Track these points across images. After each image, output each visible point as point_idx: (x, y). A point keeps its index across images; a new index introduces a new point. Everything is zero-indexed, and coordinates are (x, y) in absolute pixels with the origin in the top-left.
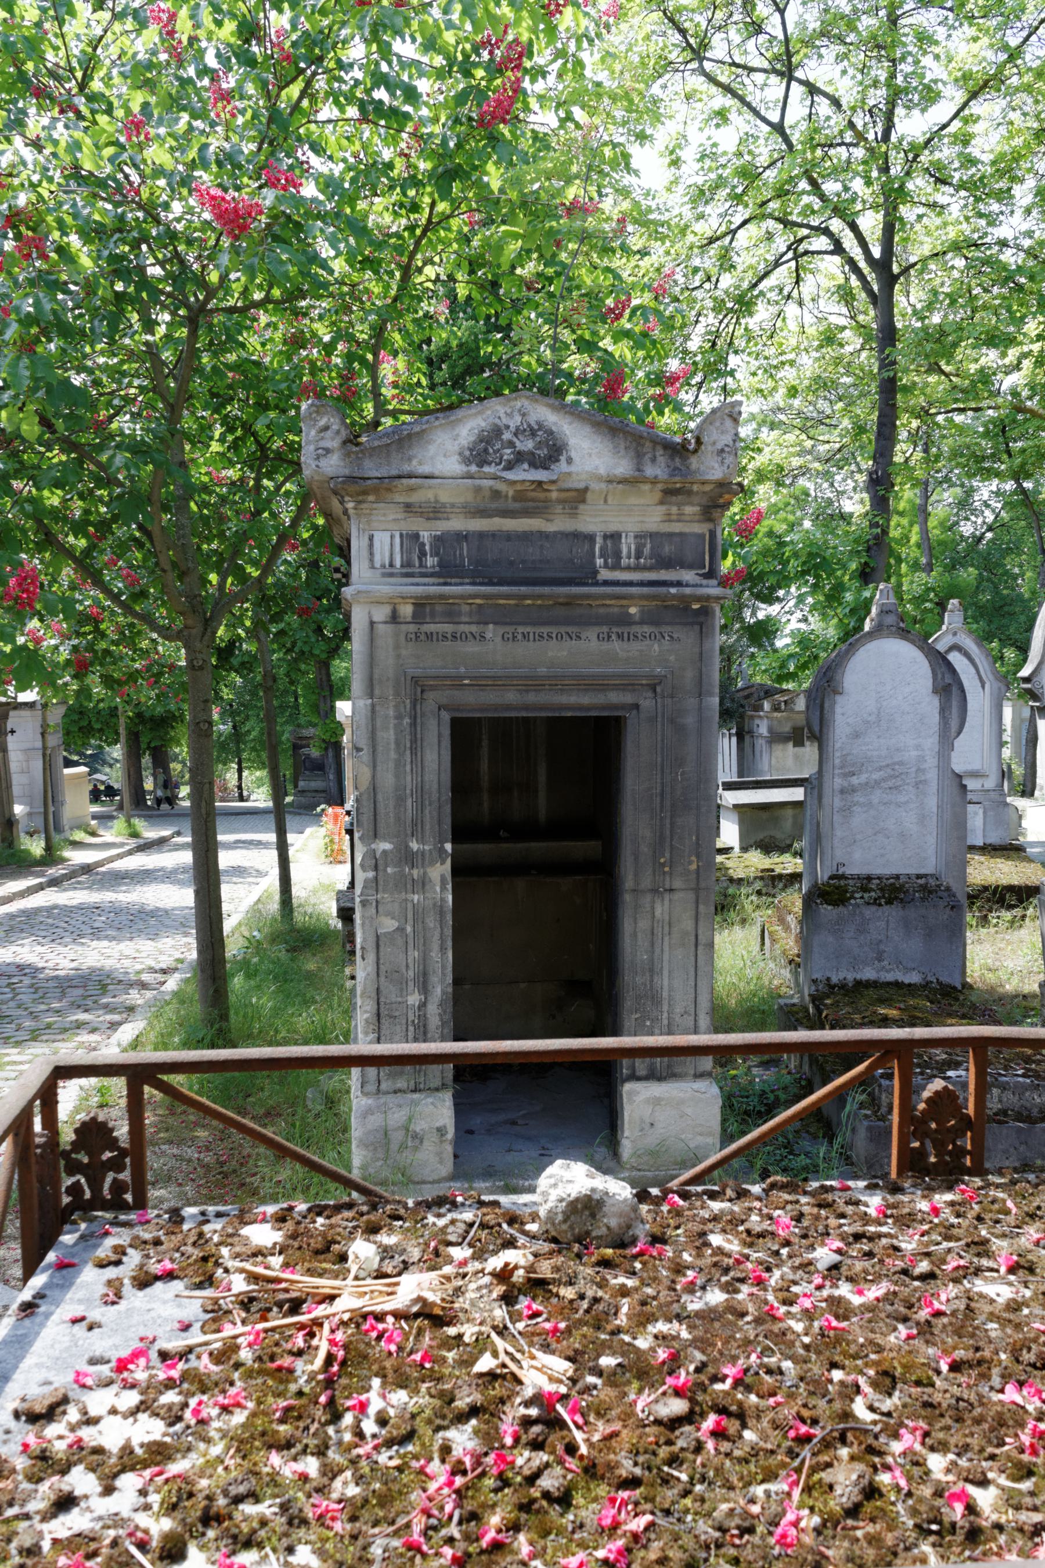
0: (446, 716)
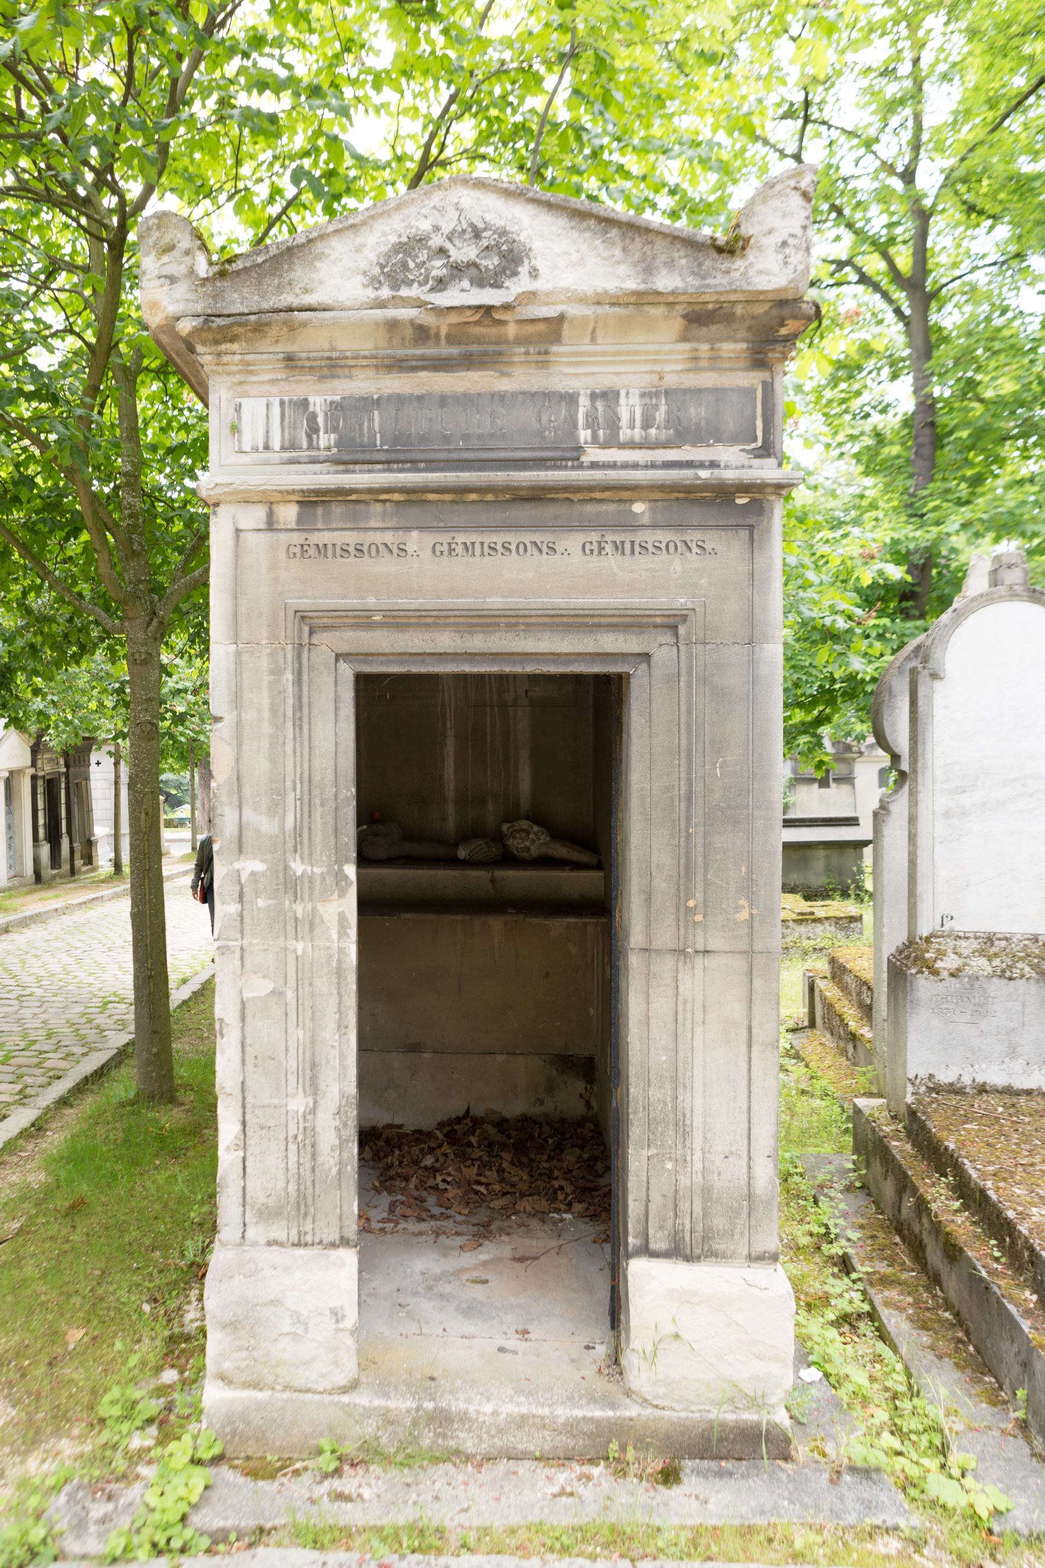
0: (347, 672)
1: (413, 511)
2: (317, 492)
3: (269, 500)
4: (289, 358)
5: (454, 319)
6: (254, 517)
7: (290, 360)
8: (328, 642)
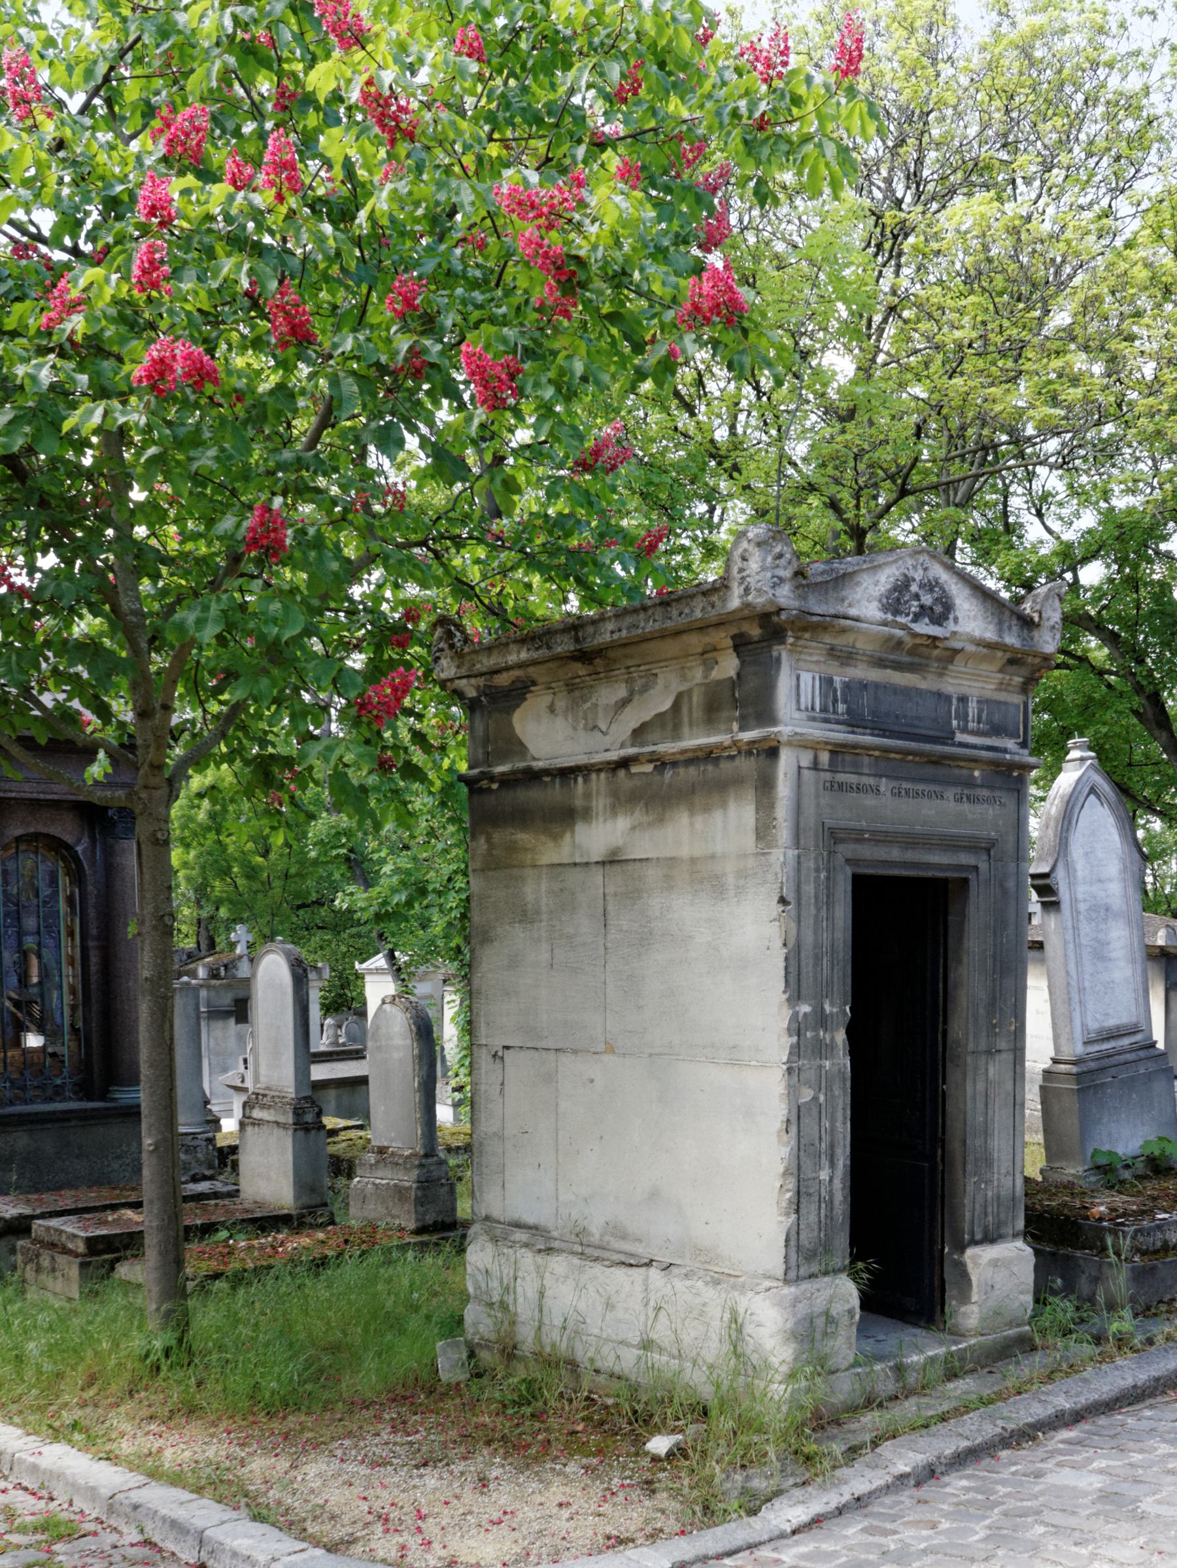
0: (849, 871)
2: (844, 746)
3: (813, 746)
8: (846, 850)
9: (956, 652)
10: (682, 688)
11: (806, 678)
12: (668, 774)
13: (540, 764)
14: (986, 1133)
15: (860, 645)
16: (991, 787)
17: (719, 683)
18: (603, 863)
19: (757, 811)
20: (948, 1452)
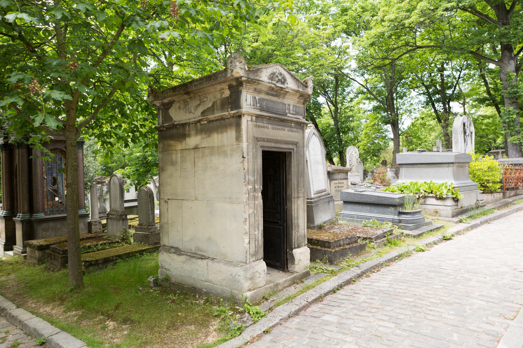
1: (269, 121)
2: (259, 115)
3: (251, 115)
4: (255, 89)
5: (278, 88)
6: (249, 118)
7: (255, 90)
9: (287, 92)
10: (214, 100)
11: (249, 96)
12: (211, 124)
13: (176, 123)
14: (298, 219)
15: (263, 88)
16: (297, 128)
17: (225, 98)
18: (194, 149)
19: (236, 132)
20: (293, 310)
